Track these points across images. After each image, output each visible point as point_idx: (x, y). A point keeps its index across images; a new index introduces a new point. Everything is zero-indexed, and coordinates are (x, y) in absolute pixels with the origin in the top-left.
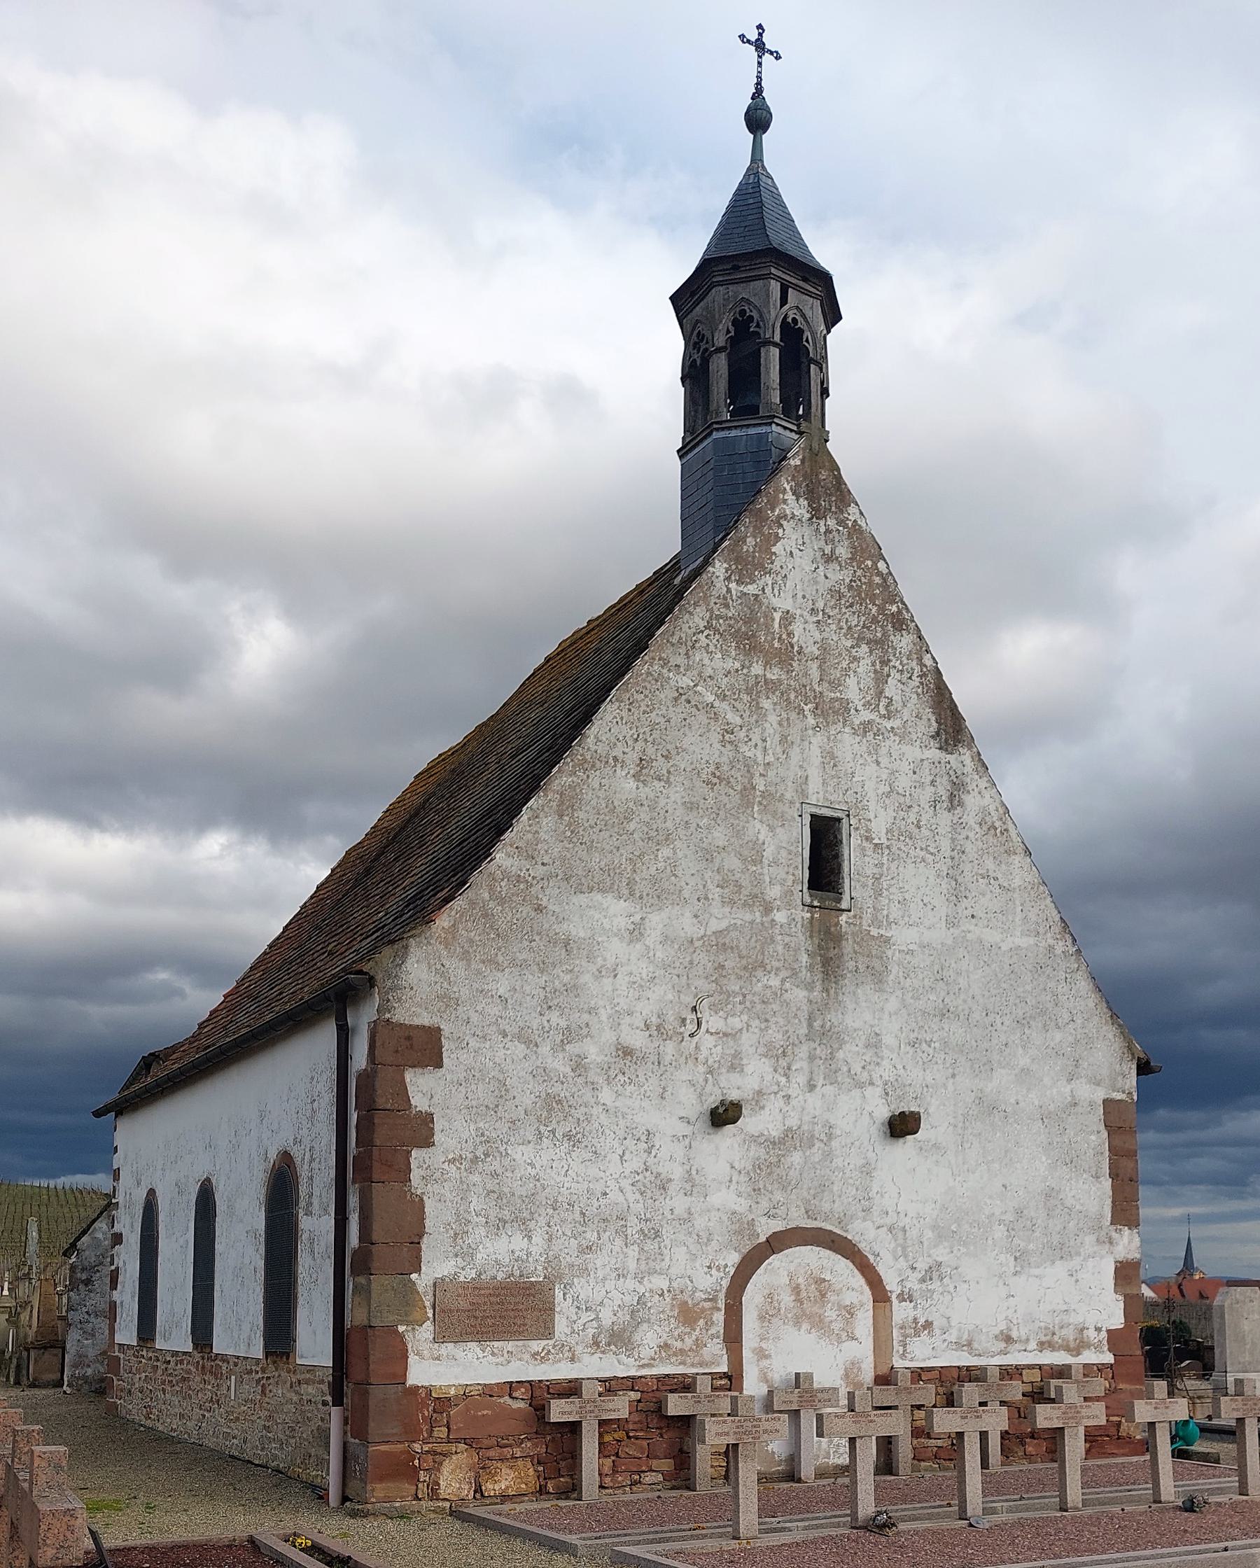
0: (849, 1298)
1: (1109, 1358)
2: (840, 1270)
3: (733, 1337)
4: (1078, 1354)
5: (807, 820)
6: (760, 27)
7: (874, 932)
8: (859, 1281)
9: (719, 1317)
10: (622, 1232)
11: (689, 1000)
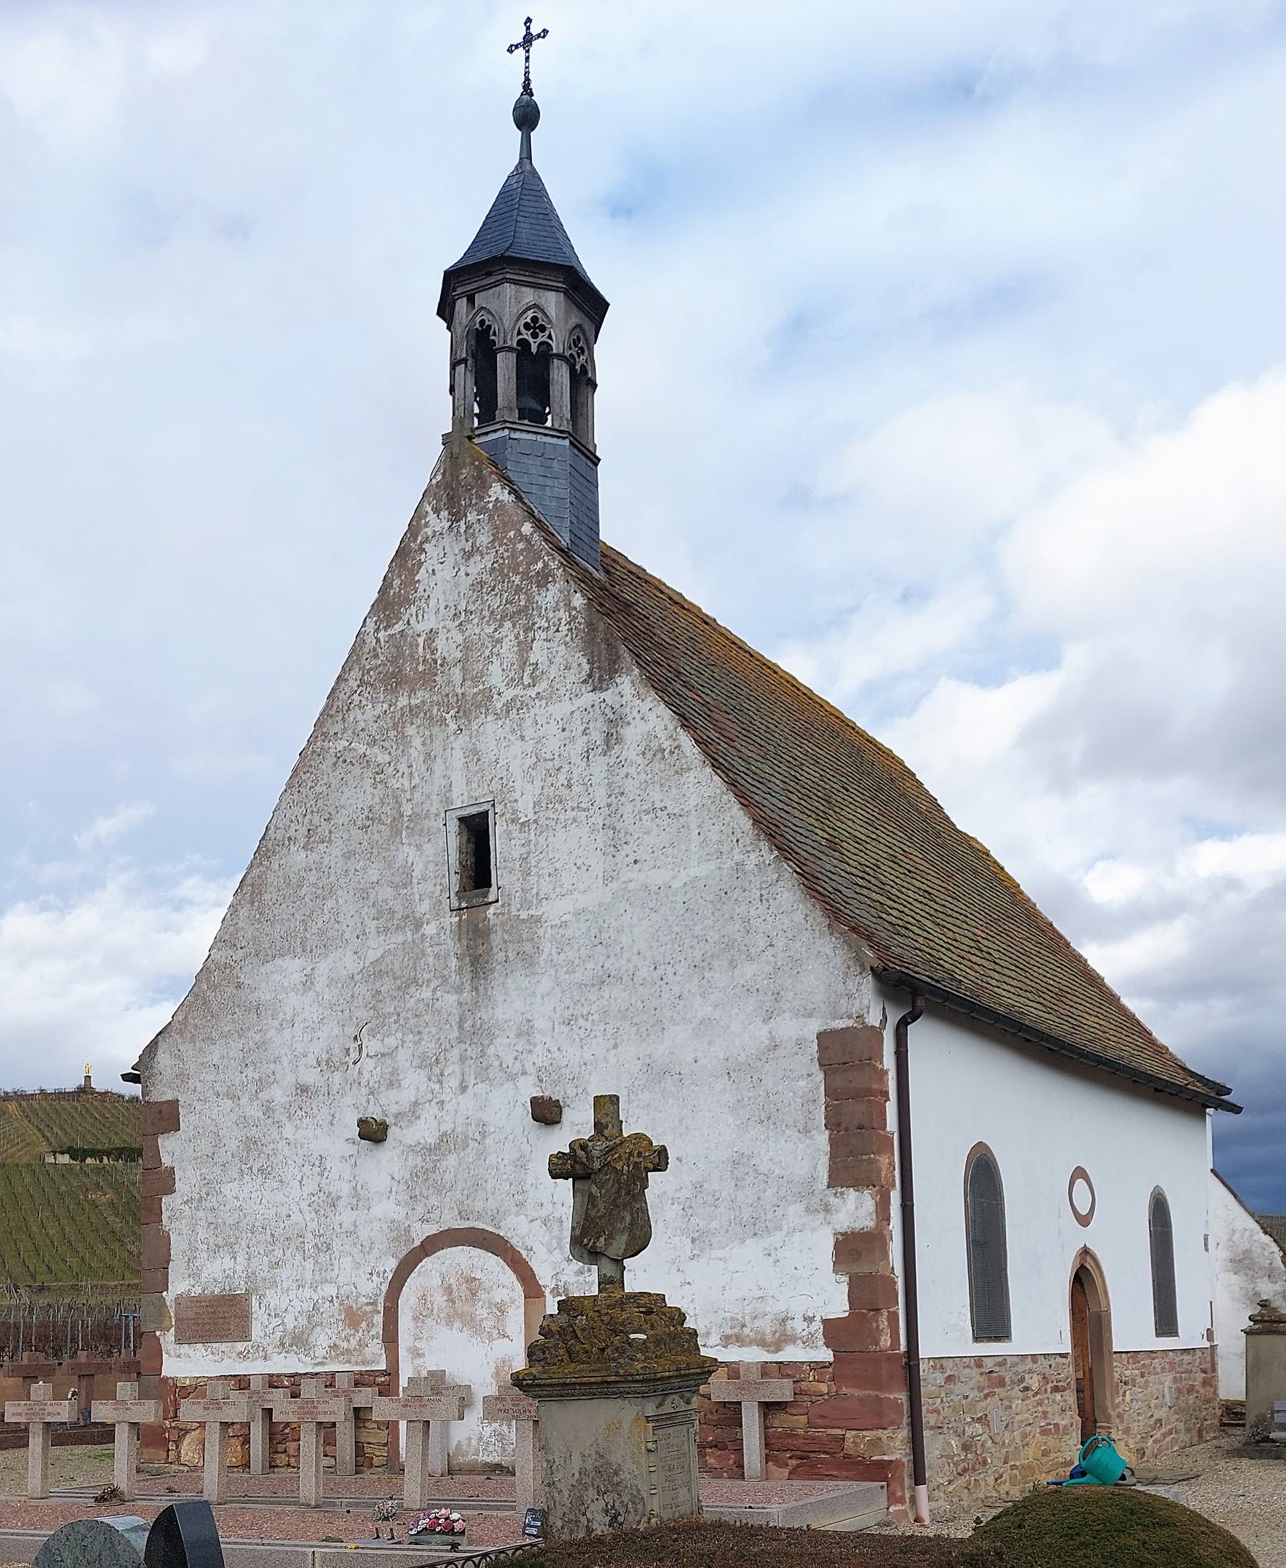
0: (499, 1295)
1: (826, 1355)
2: (492, 1267)
3: (390, 1338)
4: (778, 1350)
5: (453, 826)
6: (545, 32)
7: (524, 915)
8: (510, 1277)
9: (379, 1319)
10: (301, 1248)
11: (352, 1031)
